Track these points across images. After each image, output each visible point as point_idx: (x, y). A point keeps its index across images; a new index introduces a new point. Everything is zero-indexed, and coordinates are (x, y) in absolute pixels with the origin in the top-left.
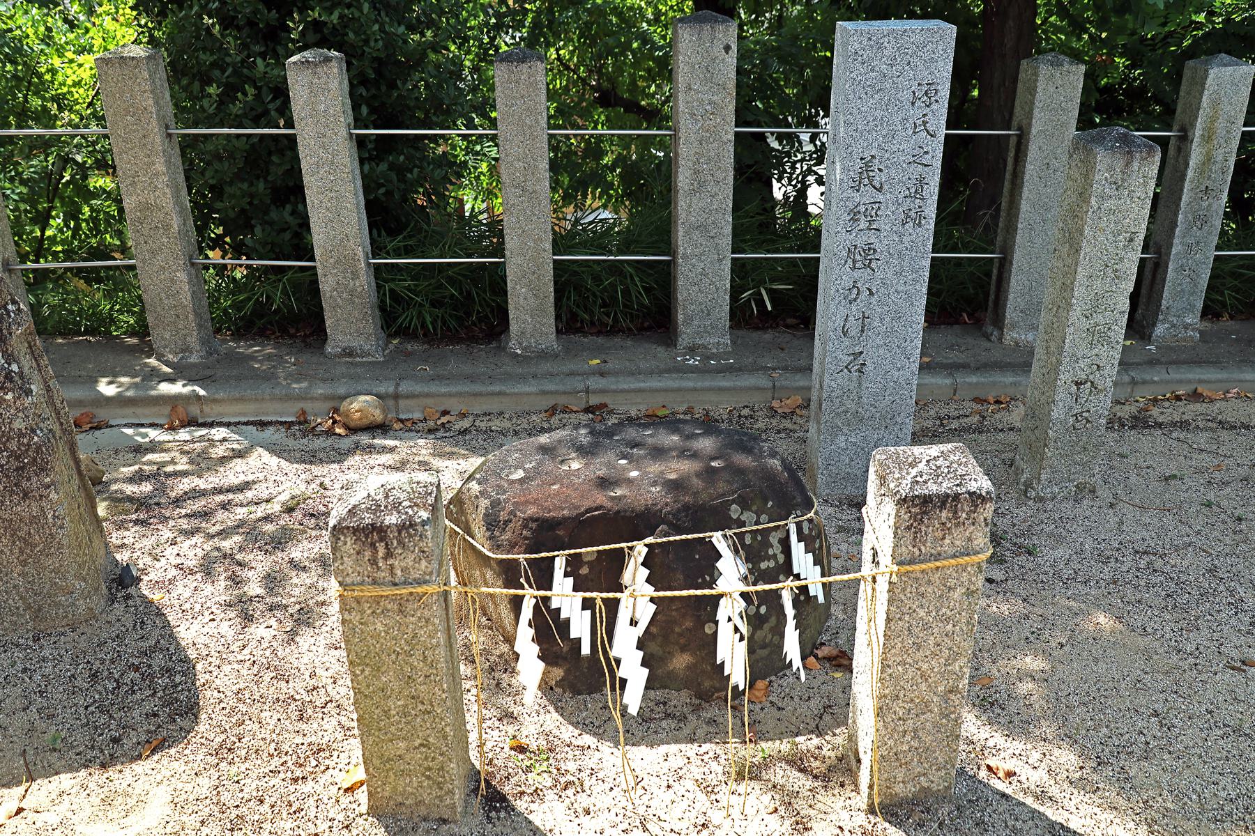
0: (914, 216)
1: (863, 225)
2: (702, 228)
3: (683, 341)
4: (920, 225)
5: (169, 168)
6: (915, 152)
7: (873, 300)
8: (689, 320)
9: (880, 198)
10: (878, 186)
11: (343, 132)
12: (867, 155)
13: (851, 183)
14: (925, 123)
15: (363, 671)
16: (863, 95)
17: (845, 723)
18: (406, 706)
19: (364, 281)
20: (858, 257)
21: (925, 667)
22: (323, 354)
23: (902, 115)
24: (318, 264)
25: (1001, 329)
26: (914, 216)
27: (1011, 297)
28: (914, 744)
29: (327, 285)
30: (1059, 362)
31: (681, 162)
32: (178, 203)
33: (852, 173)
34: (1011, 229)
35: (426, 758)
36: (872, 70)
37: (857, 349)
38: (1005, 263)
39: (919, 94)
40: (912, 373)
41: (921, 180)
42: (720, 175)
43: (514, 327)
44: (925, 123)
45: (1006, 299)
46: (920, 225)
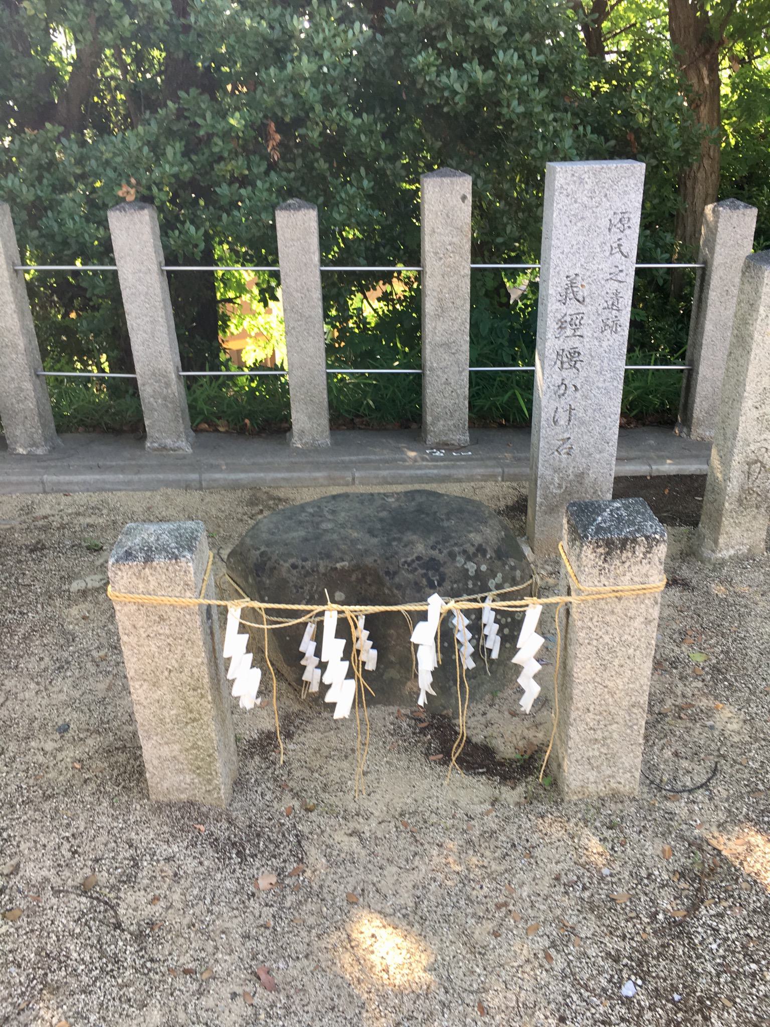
0: (611, 324)
1: (569, 332)
2: (446, 345)
3: (431, 439)
4: (616, 332)
5: (15, 298)
6: (612, 271)
7: (578, 395)
8: (437, 419)
9: (582, 309)
10: (581, 299)
11: (155, 268)
12: (572, 274)
13: (559, 298)
14: (619, 245)
15: (141, 686)
16: (568, 223)
17: (29, 286)
18: (178, 715)
19: (176, 389)
20: (565, 359)
21: (611, 684)
22: (143, 448)
23: (601, 239)
24: (137, 376)
25: (689, 428)
26: (611, 324)
27: (698, 400)
28: (604, 750)
29: (146, 391)
30: (733, 446)
31: (428, 292)
32: (23, 327)
33: (559, 289)
34: (697, 345)
35: (196, 759)
36: (576, 202)
37: (566, 435)
38: (690, 376)
39: (615, 221)
40: (612, 455)
41: (617, 293)
42: (459, 302)
43: (295, 428)
44: (619, 245)
45: (694, 402)
46: (616, 332)
